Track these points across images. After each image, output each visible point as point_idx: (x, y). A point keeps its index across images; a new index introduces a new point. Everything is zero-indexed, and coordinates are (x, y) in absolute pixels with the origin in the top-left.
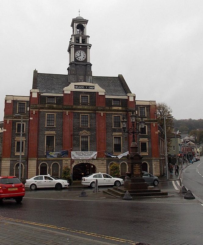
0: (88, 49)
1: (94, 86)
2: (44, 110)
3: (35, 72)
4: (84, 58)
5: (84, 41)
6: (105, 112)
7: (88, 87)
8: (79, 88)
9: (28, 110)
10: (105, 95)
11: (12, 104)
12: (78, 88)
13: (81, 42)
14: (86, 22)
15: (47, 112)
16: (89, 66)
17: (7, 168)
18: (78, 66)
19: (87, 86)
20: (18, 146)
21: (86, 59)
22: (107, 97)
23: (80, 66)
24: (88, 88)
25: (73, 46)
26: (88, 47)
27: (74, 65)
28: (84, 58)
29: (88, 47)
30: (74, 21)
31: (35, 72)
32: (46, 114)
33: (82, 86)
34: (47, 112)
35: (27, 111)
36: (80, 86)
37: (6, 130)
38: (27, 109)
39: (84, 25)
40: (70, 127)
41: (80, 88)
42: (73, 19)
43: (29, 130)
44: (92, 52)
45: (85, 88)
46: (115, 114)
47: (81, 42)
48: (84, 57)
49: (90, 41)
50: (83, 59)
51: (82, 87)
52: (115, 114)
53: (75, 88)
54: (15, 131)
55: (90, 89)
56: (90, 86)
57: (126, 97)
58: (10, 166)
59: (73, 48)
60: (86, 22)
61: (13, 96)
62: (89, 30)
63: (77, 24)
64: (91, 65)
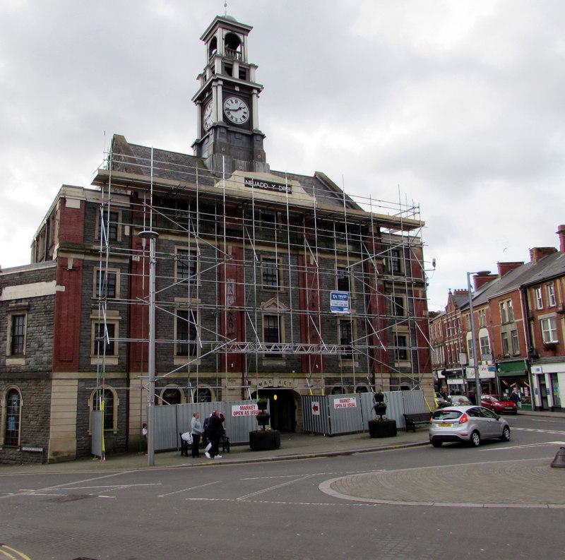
0: (255, 97)
2: (170, 238)
4: (244, 117)
5: (244, 74)
9: (127, 233)
11: (83, 212)
13: (236, 73)
14: (246, 30)
16: (259, 138)
17: (67, 402)
18: (232, 136)
21: (250, 122)
23: (238, 136)
25: (221, 83)
26: (255, 91)
27: (223, 131)
28: (244, 117)
29: (255, 91)
30: (220, 22)
32: (176, 248)
33: (264, 182)
34: (177, 243)
35: (124, 236)
37: (63, 289)
38: (123, 230)
39: (241, 37)
40: (185, 375)
42: (218, 17)
43: (130, 292)
44: (259, 102)
47: (236, 73)
48: (245, 115)
49: (256, 77)
50: (243, 119)
53: (247, 186)
54: (90, 291)
56: (7, 425)
58: (78, 397)
59: (220, 89)
60: (246, 30)
61: (84, 189)
62: (252, 50)
63: (225, 32)
64: (263, 137)
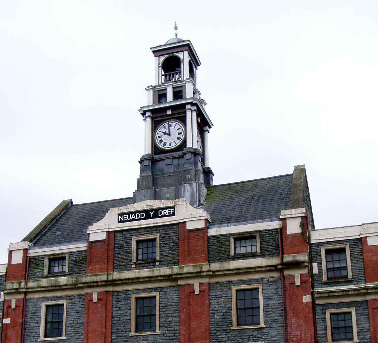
1: (174, 207)
3: (139, 161)
6: (206, 280)
7: (156, 213)
8: (131, 221)
10: (207, 227)
12: (128, 221)
15: (44, 299)
19: (152, 210)
20: (56, 299)
22: (213, 232)
24: (156, 216)
28: (161, 141)
30: (171, 136)
31: (139, 161)
33: (140, 212)
36: (135, 213)
41: (133, 220)
45: (148, 217)
46: (239, 282)
51: (140, 215)
52: (239, 282)
53: (121, 221)
55: (163, 216)
56: (162, 209)
57: (276, 225)
